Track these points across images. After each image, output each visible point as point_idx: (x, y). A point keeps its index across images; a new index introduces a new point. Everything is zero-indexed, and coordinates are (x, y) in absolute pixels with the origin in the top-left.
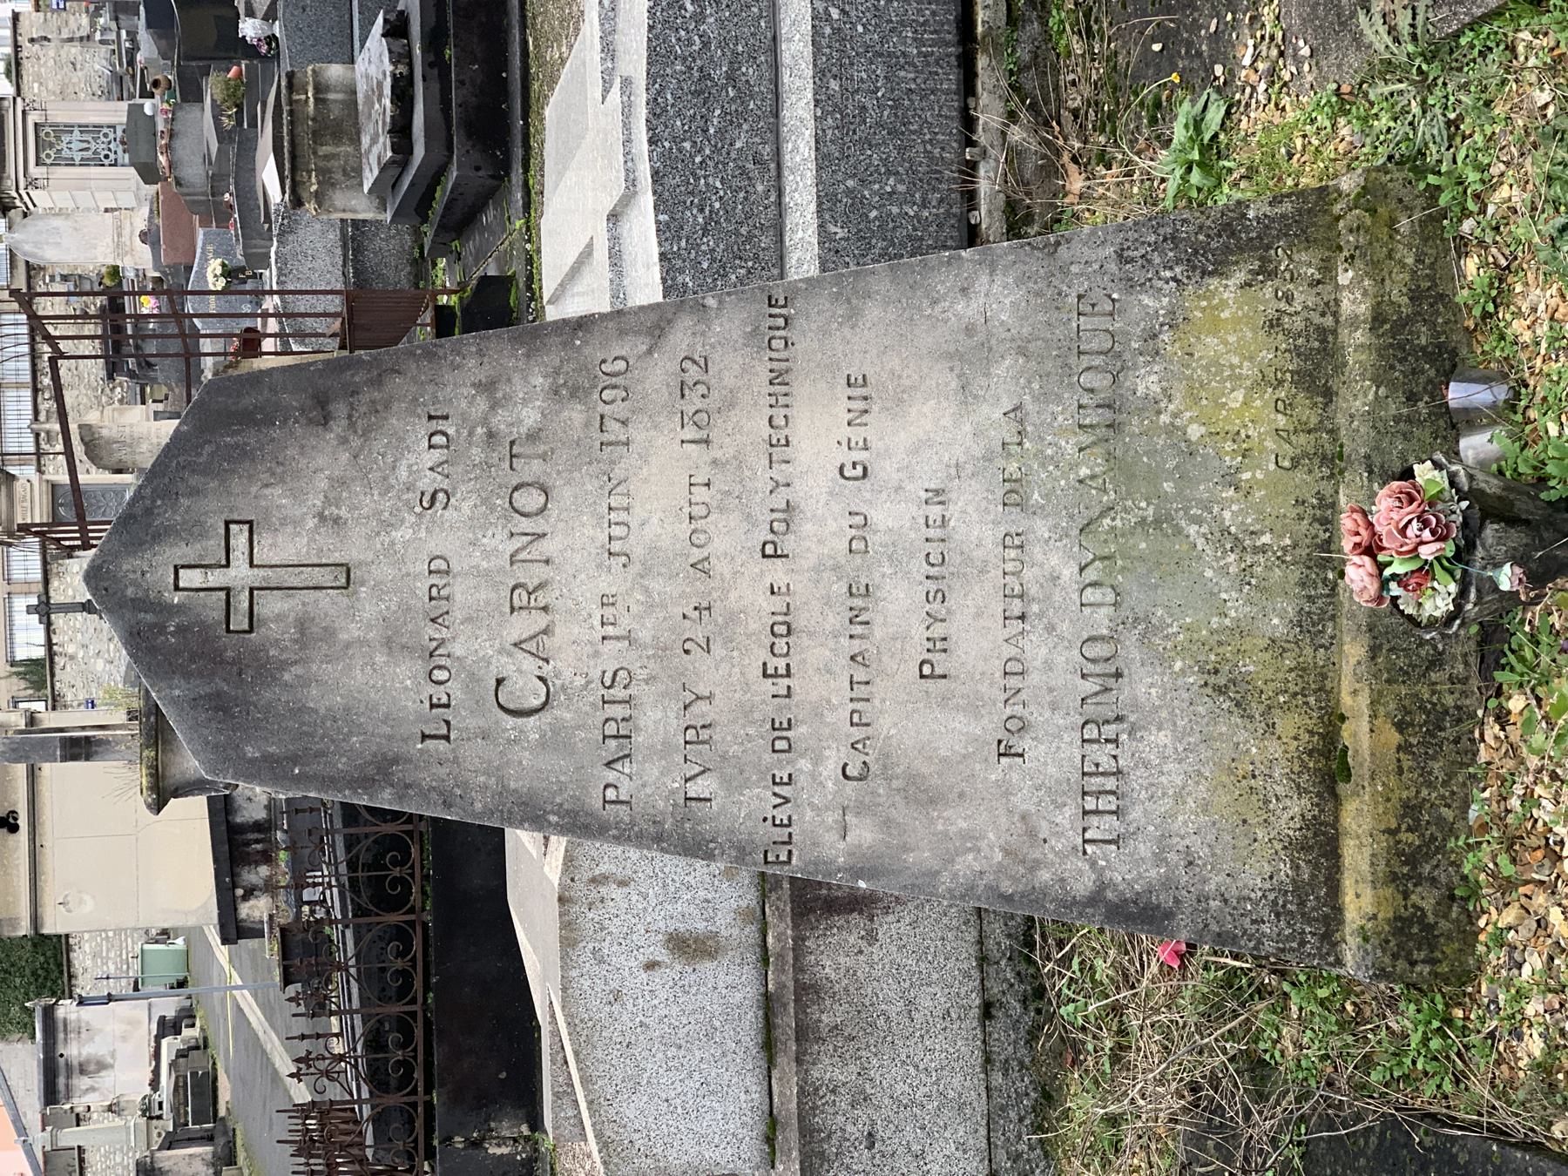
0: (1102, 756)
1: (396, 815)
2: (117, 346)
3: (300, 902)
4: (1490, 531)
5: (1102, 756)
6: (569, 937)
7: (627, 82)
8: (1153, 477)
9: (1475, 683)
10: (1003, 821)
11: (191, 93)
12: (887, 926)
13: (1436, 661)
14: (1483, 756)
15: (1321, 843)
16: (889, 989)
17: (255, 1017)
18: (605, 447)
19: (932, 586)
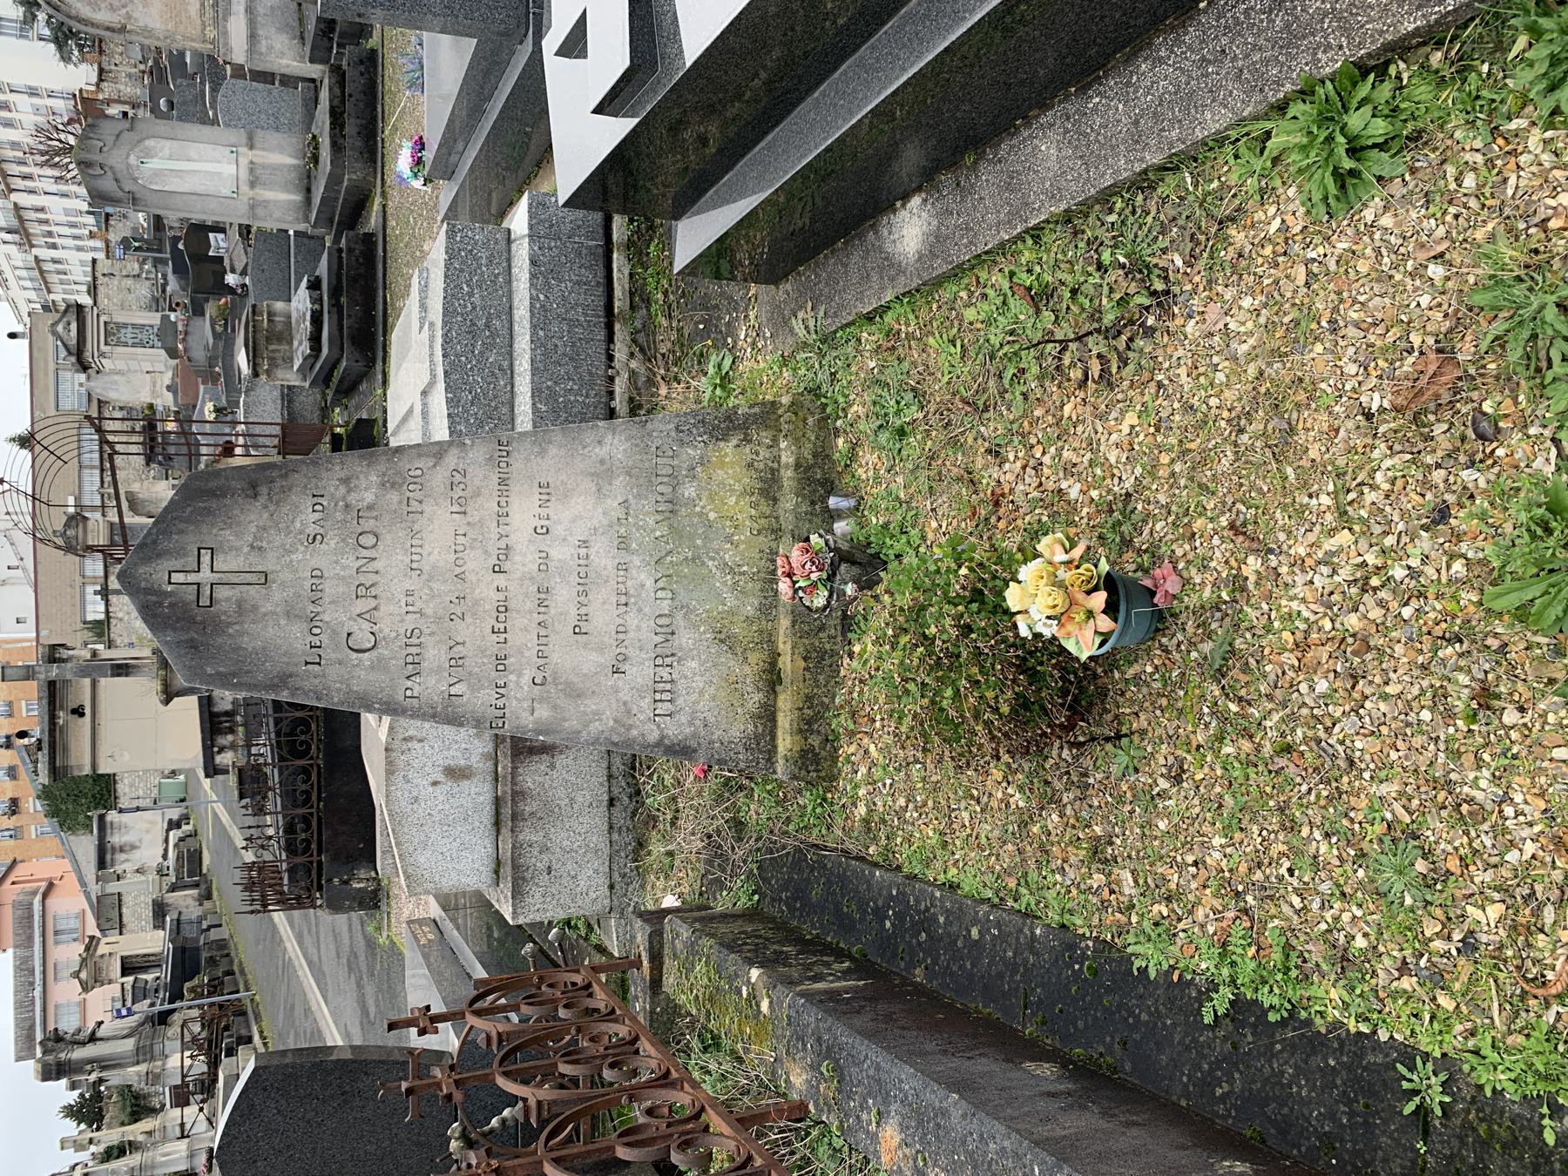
0: (664, 673)
1: (303, 707)
2: (152, 449)
3: (250, 754)
4: (843, 567)
5: (664, 673)
6: (391, 770)
7: (432, 324)
8: (692, 537)
9: (839, 638)
10: (614, 705)
11: (198, 311)
12: (560, 761)
13: (822, 628)
14: (842, 673)
15: (768, 715)
16: (561, 793)
17: (225, 818)
18: (409, 514)
19: (581, 588)
